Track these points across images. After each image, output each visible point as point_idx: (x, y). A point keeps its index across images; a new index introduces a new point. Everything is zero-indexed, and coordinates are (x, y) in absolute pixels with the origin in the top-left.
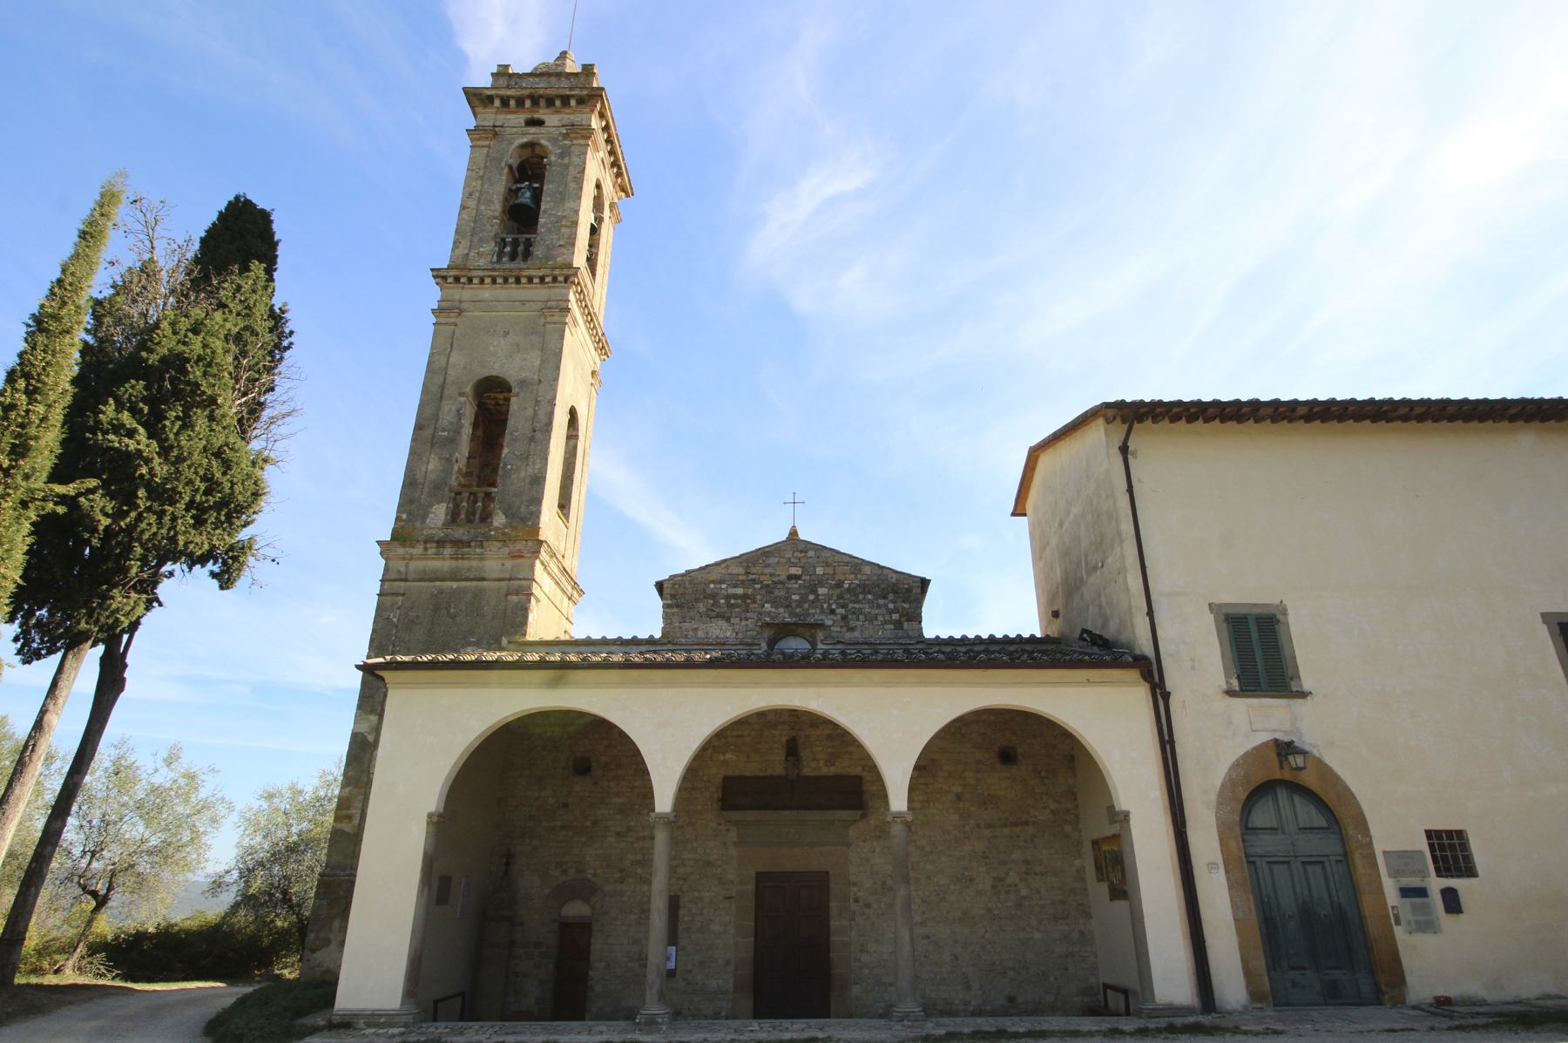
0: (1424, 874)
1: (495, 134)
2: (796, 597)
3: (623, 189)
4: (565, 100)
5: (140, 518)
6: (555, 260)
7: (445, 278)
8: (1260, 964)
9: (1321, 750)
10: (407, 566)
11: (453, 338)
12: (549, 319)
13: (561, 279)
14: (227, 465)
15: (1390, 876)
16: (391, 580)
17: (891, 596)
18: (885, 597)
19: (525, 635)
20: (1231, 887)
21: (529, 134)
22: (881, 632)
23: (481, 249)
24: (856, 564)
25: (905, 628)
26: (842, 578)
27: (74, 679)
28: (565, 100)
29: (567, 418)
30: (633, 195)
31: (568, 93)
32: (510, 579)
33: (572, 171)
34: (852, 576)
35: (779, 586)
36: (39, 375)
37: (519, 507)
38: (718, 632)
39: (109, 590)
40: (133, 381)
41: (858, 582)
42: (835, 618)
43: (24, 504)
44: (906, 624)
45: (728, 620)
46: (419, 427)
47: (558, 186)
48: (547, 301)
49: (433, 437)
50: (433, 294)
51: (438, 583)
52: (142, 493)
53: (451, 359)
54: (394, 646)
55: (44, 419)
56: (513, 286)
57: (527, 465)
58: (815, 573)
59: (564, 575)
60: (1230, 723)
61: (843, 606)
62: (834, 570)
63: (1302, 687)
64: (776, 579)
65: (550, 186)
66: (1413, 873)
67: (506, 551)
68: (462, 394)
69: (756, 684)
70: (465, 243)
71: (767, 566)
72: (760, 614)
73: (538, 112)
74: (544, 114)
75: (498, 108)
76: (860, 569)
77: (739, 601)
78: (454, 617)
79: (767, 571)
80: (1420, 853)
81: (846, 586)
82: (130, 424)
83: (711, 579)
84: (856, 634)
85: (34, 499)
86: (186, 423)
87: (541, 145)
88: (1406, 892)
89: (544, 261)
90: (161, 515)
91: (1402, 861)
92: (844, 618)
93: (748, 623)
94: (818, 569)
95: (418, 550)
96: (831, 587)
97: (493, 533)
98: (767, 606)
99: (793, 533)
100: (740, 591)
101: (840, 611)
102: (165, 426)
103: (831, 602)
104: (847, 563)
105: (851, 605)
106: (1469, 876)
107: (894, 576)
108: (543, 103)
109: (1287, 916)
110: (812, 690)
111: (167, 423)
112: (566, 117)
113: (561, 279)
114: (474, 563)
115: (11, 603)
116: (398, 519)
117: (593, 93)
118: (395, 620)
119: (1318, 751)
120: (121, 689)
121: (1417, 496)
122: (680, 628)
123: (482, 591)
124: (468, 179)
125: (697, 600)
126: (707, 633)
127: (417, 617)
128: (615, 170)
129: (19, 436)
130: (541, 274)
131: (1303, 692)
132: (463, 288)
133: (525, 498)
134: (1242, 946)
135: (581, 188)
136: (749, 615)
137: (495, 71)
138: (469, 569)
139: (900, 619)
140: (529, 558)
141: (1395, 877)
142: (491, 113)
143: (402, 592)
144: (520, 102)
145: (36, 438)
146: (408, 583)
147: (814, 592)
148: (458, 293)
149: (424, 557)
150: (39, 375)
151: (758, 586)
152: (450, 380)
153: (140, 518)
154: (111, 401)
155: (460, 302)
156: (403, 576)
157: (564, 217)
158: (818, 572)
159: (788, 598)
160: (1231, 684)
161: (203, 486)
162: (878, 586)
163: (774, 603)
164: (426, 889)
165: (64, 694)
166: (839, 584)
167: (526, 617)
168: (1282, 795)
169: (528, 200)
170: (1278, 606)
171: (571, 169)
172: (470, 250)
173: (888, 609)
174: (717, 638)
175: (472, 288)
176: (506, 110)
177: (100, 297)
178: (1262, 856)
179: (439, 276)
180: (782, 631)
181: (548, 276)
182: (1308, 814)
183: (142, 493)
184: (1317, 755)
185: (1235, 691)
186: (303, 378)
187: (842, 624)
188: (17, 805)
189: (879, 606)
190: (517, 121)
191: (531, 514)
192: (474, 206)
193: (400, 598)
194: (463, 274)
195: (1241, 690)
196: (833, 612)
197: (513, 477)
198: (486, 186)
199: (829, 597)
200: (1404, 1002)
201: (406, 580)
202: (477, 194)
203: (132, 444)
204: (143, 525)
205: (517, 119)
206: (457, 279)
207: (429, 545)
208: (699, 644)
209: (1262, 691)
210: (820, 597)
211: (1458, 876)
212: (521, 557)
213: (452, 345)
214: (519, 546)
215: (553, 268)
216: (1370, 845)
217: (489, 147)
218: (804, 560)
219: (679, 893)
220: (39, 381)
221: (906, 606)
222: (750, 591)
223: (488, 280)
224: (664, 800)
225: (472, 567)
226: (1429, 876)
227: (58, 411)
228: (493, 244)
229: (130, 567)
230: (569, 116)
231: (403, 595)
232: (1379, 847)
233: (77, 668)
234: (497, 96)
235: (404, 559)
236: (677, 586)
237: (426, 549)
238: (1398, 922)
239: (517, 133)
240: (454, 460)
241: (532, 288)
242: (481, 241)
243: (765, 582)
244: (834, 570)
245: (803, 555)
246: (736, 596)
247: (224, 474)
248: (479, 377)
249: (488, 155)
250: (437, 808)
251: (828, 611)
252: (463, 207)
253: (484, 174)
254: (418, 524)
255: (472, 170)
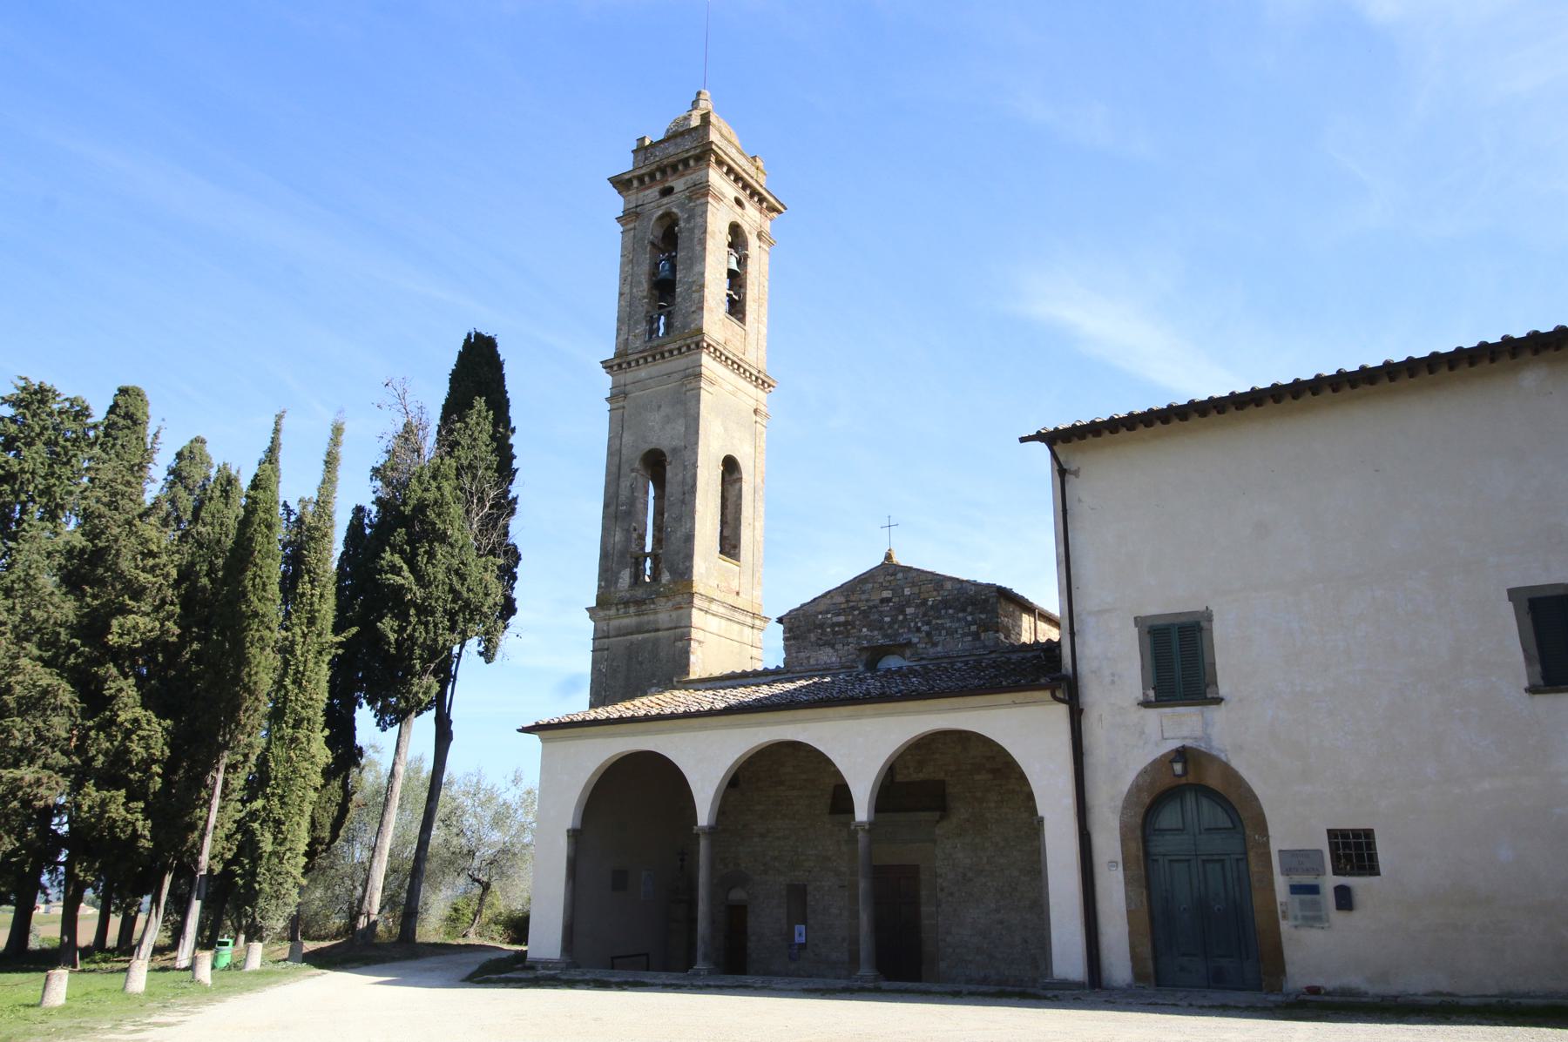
0: (1319, 872)
1: (637, 215)
2: (887, 619)
3: (773, 209)
4: (685, 162)
5: (414, 630)
6: (690, 328)
7: (611, 367)
8: (1146, 950)
9: (1229, 756)
10: (608, 625)
11: (622, 420)
12: (688, 387)
13: (693, 346)
14: (463, 578)
15: (1282, 874)
16: (599, 638)
17: (969, 609)
18: (964, 610)
19: (688, 674)
20: (1127, 883)
21: (663, 205)
22: (960, 645)
23: (637, 331)
24: (938, 581)
25: (982, 638)
26: (926, 595)
27: (409, 740)
28: (685, 162)
29: (718, 471)
30: (786, 209)
31: (686, 155)
32: (676, 628)
33: (697, 232)
34: (935, 593)
35: (875, 610)
36: (314, 569)
37: (678, 564)
38: (825, 658)
39: (412, 679)
40: (399, 530)
41: (940, 598)
42: (921, 636)
43: (320, 653)
44: (983, 635)
45: (833, 646)
46: (606, 506)
47: (688, 253)
48: (686, 369)
49: (616, 513)
50: (606, 381)
51: (629, 637)
52: (412, 612)
53: (623, 440)
54: (606, 692)
55: (322, 596)
56: (660, 361)
57: (681, 526)
58: (903, 595)
59: (734, 611)
60: (1142, 733)
61: (928, 623)
62: (920, 589)
63: (1218, 693)
64: (871, 604)
65: (682, 254)
66: (1307, 871)
67: (670, 604)
68: (632, 470)
69: (760, 724)
70: (625, 328)
71: (864, 592)
72: (859, 638)
73: (667, 181)
74: (673, 181)
75: (637, 188)
76: (942, 585)
77: (842, 628)
78: (641, 663)
79: (864, 597)
80: (1320, 852)
81: (930, 603)
82: (400, 563)
83: (819, 610)
84: (939, 649)
85: (324, 650)
86: (431, 555)
87: (673, 213)
88: (1295, 889)
89: (682, 330)
90: (426, 624)
91: (1297, 860)
92: (928, 634)
93: (849, 647)
94: (906, 590)
95: (613, 612)
96: (917, 606)
97: (662, 589)
98: (864, 630)
99: (888, 557)
100: (842, 619)
101: (925, 628)
102: (418, 561)
103: (917, 620)
104: (931, 580)
105: (934, 622)
106: (1371, 875)
107: (973, 588)
108: (669, 171)
109: (1182, 909)
110: (799, 726)
111: (419, 558)
112: (688, 177)
113: (693, 346)
114: (652, 617)
115: (324, 715)
116: (599, 587)
117: (705, 148)
118: (604, 670)
119: (1226, 755)
120: (451, 739)
121: (1377, 471)
122: (797, 657)
123: (656, 642)
124: (622, 265)
125: (809, 631)
126: (817, 660)
127: (618, 666)
128: (756, 199)
129: (310, 612)
130: (677, 346)
131: (1218, 698)
132: (626, 372)
133: (681, 555)
134: (1131, 934)
135: (705, 249)
136: (850, 640)
137: (635, 148)
138: (648, 622)
139: (977, 631)
140: (687, 608)
141: (1288, 875)
142: (632, 194)
143: (606, 647)
144: (652, 176)
145: (319, 611)
146: (611, 640)
147: (902, 612)
148: (629, 376)
149: (618, 617)
150: (314, 569)
151: (856, 612)
152: (624, 459)
153: (414, 630)
154: (387, 548)
155: (625, 385)
156: (606, 634)
157: (694, 282)
158: (906, 593)
159: (881, 621)
160: (1147, 695)
161: (450, 597)
162: (958, 599)
163: (871, 628)
164: (570, 882)
165: (403, 751)
166: (925, 602)
167: (688, 659)
168: (1190, 800)
169: (667, 272)
170: (1203, 612)
171: (696, 231)
172: (629, 335)
173: (967, 621)
174: (825, 664)
175: (632, 371)
176: (644, 187)
177: (378, 465)
178: (1164, 855)
179: (608, 366)
180: (874, 655)
181: (683, 346)
182: (1211, 814)
183: (412, 612)
184: (1224, 759)
185: (1151, 702)
186: (521, 484)
187: (926, 640)
188: (388, 827)
189: (959, 620)
190: (652, 196)
191: (687, 568)
192: (628, 291)
193: (606, 652)
194: (623, 360)
195: (1156, 701)
196: (918, 630)
197: (673, 538)
198: (635, 268)
199: (915, 615)
200: (1281, 990)
201: (608, 637)
202: (629, 278)
203: (400, 580)
204: (417, 634)
205: (653, 193)
206: (620, 365)
207: (619, 607)
208: (810, 671)
209: (1177, 700)
210: (908, 617)
211: (1359, 875)
212: (681, 608)
213: (622, 427)
214: (678, 599)
215: (685, 339)
216: (1266, 845)
217: (635, 228)
218: (894, 583)
219: (806, 883)
220: (315, 573)
221: (983, 616)
222: (850, 618)
223: (641, 361)
224: (704, 816)
225: (650, 621)
226: (1324, 874)
227: (331, 585)
228: (644, 324)
229: (414, 665)
230: (691, 176)
231: (607, 649)
232: (1275, 847)
233: (409, 732)
234: (634, 177)
235: (605, 620)
236: (793, 620)
237: (618, 610)
238: (1285, 917)
239: (654, 208)
240: (632, 529)
241: (674, 360)
242: (637, 323)
243: (863, 608)
244: (920, 589)
245: (893, 578)
246: (838, 624)
247: (463, 584)
248: (645, 451)
249: (634, 236)
250: (573, 823)
251: (915, 629)
252: (621, 294)
253: (633, 257)
254: (613, 589)
255: (625, 255)
